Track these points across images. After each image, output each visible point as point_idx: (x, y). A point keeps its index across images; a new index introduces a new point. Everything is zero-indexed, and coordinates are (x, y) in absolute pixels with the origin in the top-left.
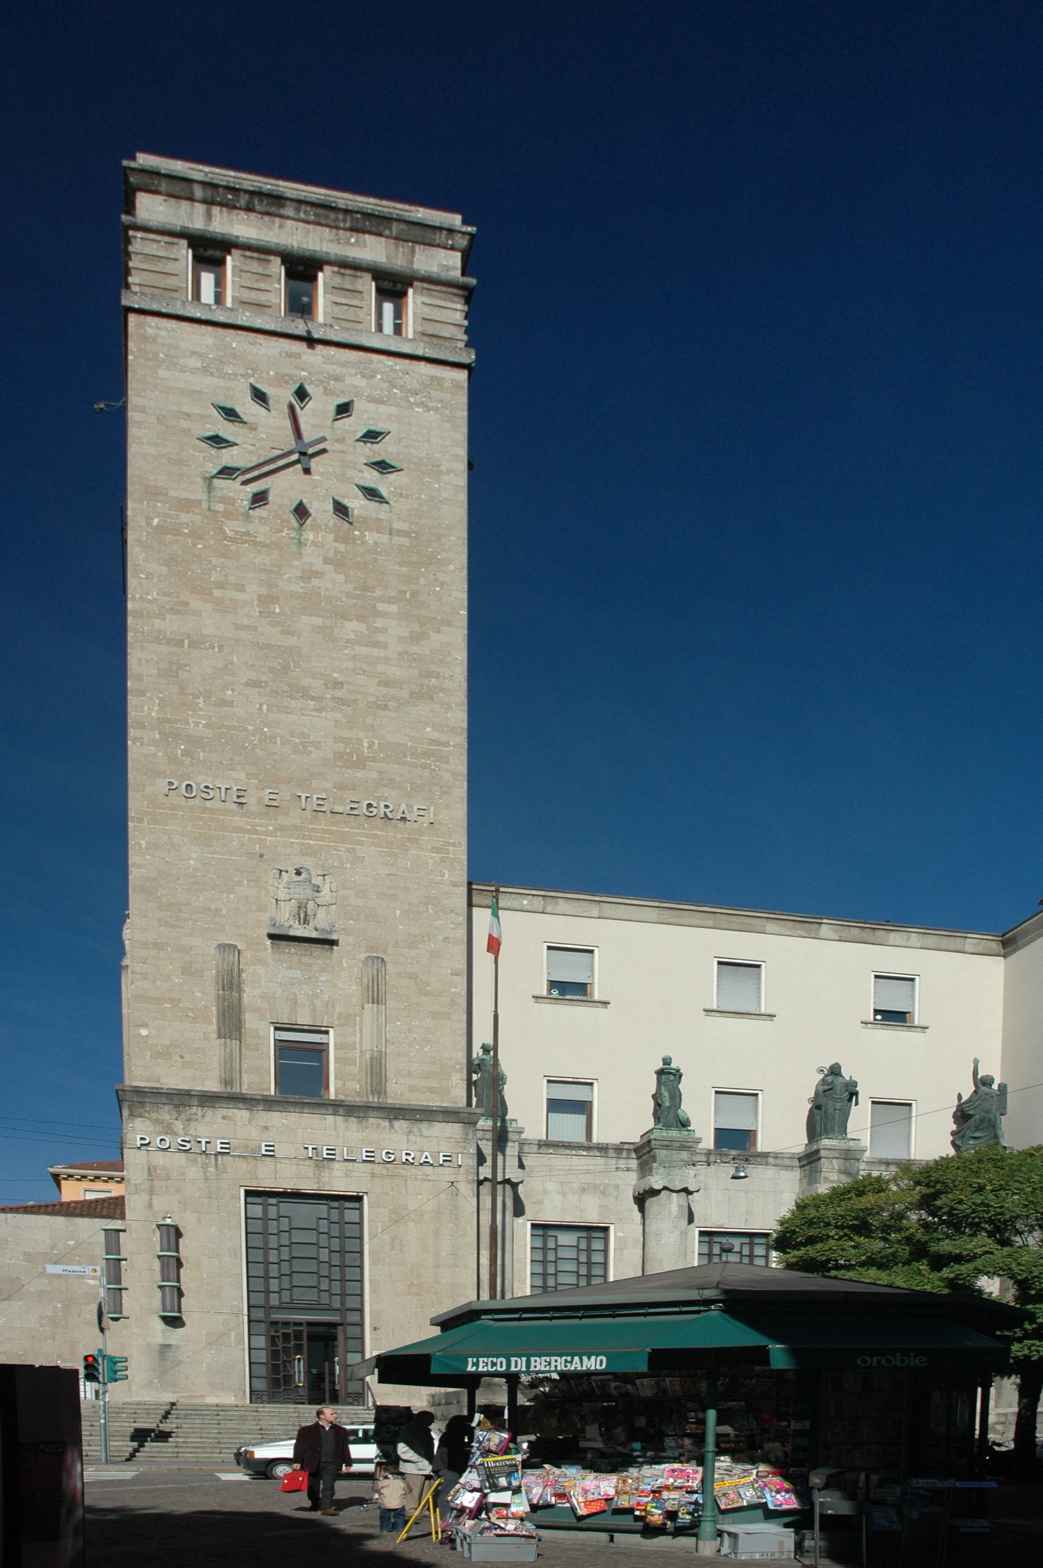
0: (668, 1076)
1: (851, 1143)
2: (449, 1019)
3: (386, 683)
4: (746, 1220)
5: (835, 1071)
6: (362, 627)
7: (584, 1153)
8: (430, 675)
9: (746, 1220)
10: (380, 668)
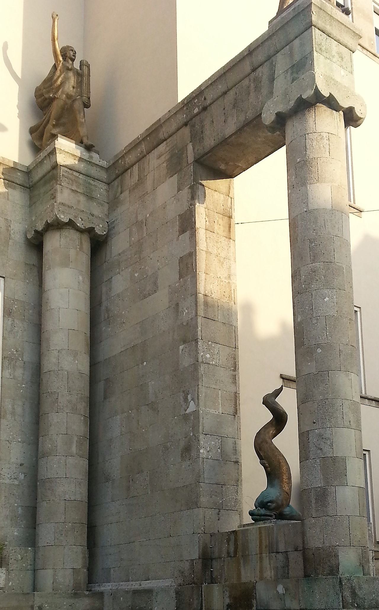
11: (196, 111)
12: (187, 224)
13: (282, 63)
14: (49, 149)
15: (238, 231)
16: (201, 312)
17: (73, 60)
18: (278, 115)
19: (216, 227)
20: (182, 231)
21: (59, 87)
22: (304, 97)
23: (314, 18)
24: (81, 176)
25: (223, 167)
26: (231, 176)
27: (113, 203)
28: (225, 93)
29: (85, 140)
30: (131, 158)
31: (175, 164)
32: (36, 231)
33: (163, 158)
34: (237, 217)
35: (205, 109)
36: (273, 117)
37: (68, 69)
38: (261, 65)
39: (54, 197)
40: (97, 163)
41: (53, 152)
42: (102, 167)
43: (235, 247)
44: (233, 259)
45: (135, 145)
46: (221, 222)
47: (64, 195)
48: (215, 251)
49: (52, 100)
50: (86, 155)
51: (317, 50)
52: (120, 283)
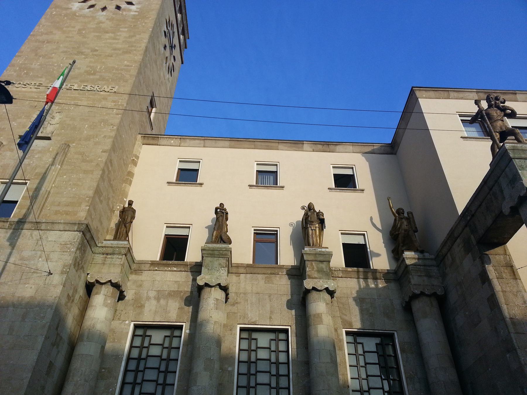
0: (221, 213)
1: (323, 250)
2: (92, 174)
3: (115, 49)
4: (270, 318)
5: (310, 207)
6: (112, 35)
7: (175, 269)
8: (132, 46)
9: (270, 318)
10: (114, 45)
11: (469, 218)
12: (485, 278)
13: (504, 182)
14: (401, 259)
15: (521, 273)
16: (512, 330)
17: (403, 214)
18: (511, 208)
19: (504, 276)
20: (483, 283)
21: (400, 228)
22: (522, 195)
23: (511, 155)
24: (422, 267)
25: (496, 241)
26: (503, 242)
27: (444, 276)
28: (480, 205)
29: (419, 248)
30: (445, 250)
31: (468, 248)
32: (406, 302)
33: (460, 246)
34: (517, 264)
35: (473, 216)
36: (509, 210)
37: (402, 218)
38: (494, 185)
39: (410, 282)
40: (429, 257)
41: (404, 260)
42: (432, 259)
43: (522, 283)
44: (523, 291)
45: (445, 243)
46: (506, 271)
47: (415, 279)
48: (508, 289)
49: (399, 234)
50: (421, 256)
51: (521, 169)
52: (460, 320)
